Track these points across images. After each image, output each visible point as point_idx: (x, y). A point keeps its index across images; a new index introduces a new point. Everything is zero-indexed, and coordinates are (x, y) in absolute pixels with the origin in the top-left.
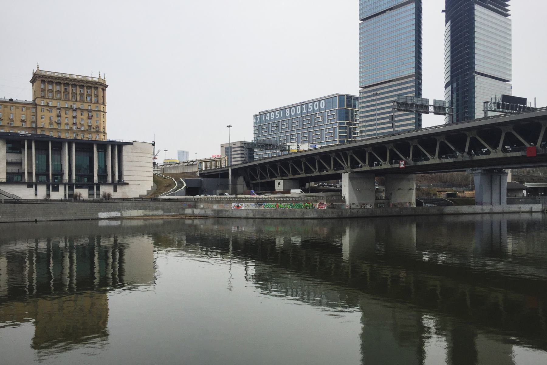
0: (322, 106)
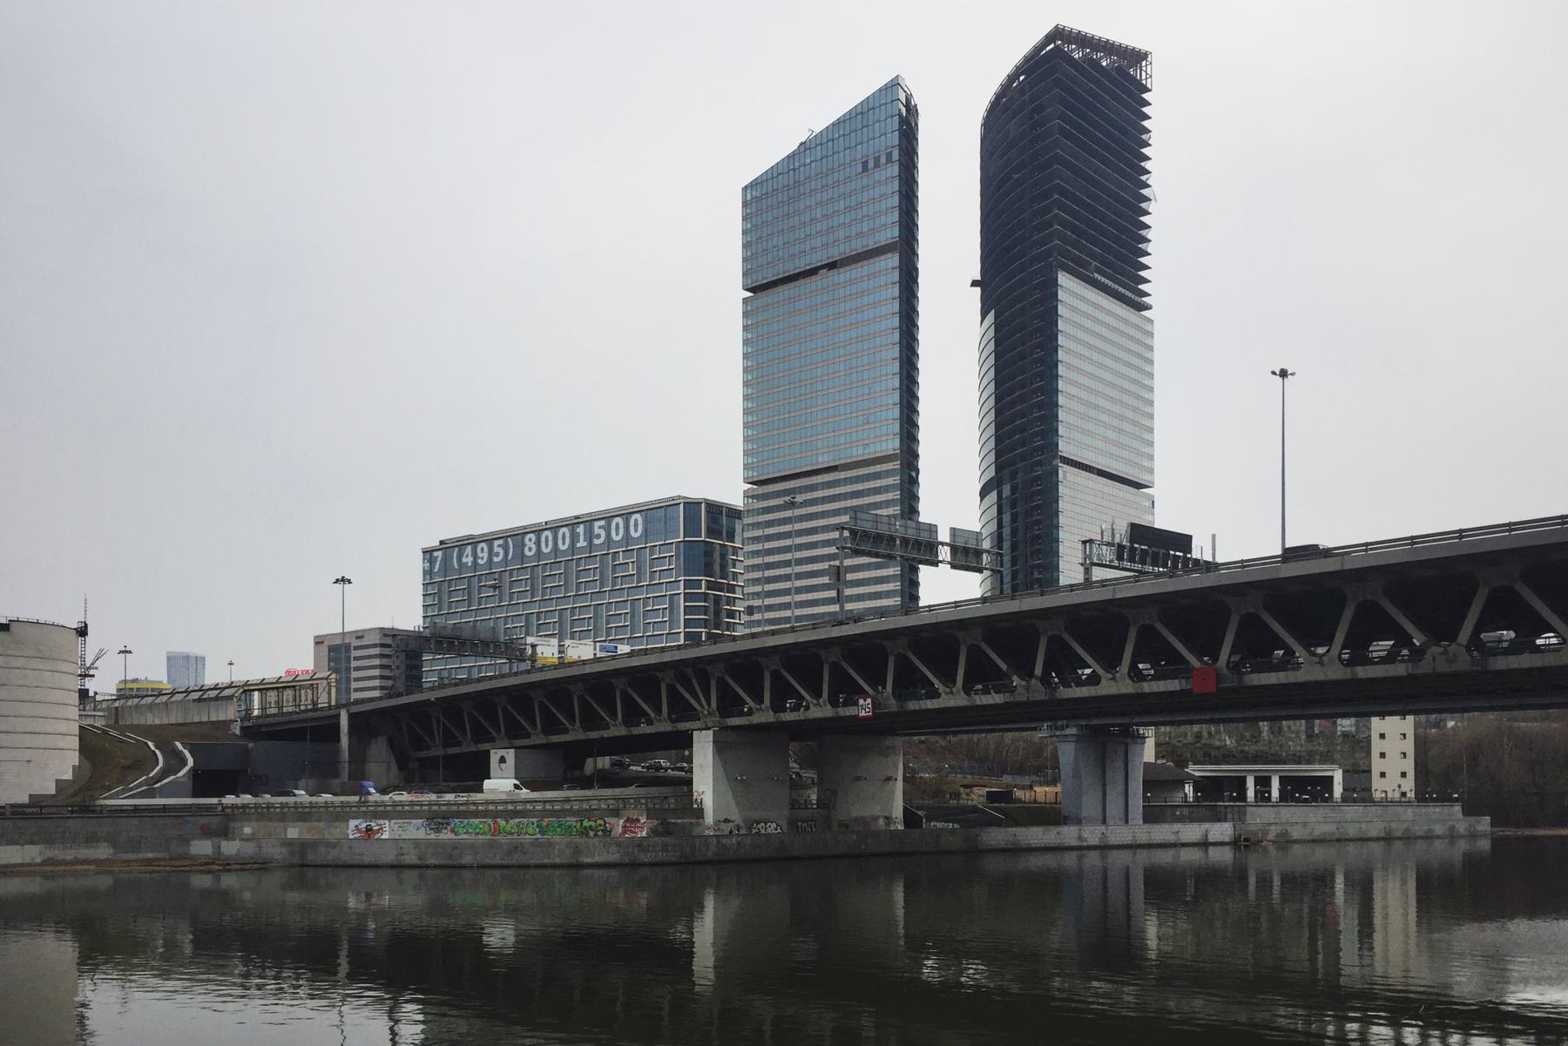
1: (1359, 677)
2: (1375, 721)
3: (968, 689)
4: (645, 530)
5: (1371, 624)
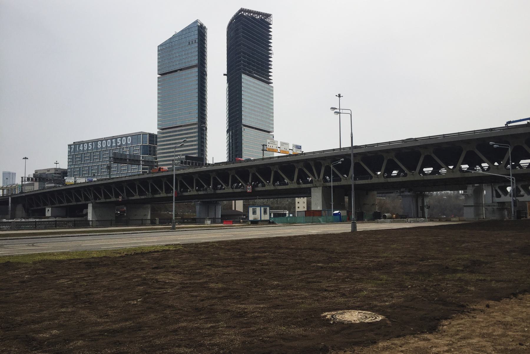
0: (129, 141)
1: (389, 181)
2: (296, 199)
3: (274, 184)
4: (132, 141)
5: (344, 168)
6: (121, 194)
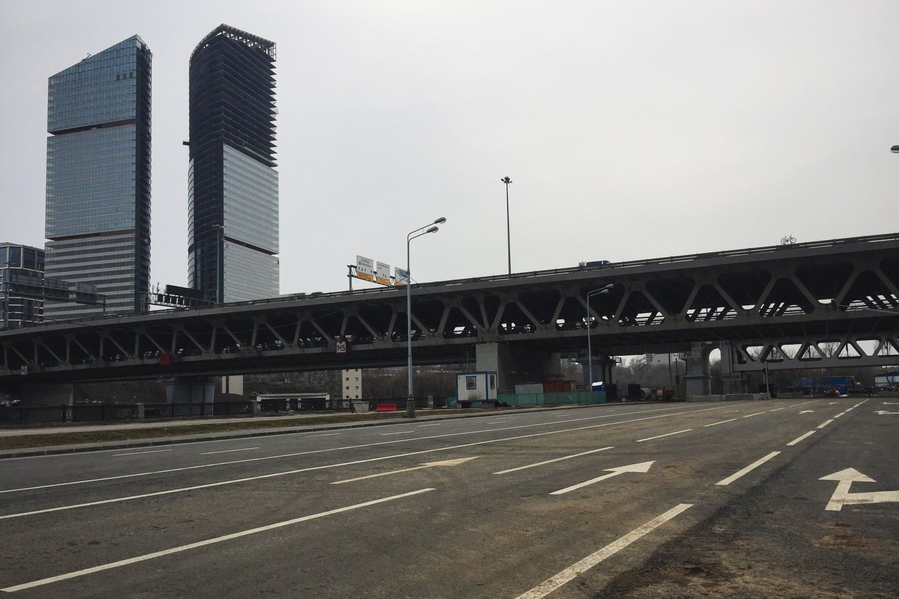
2: (344, 371)
6: (26, 361)
